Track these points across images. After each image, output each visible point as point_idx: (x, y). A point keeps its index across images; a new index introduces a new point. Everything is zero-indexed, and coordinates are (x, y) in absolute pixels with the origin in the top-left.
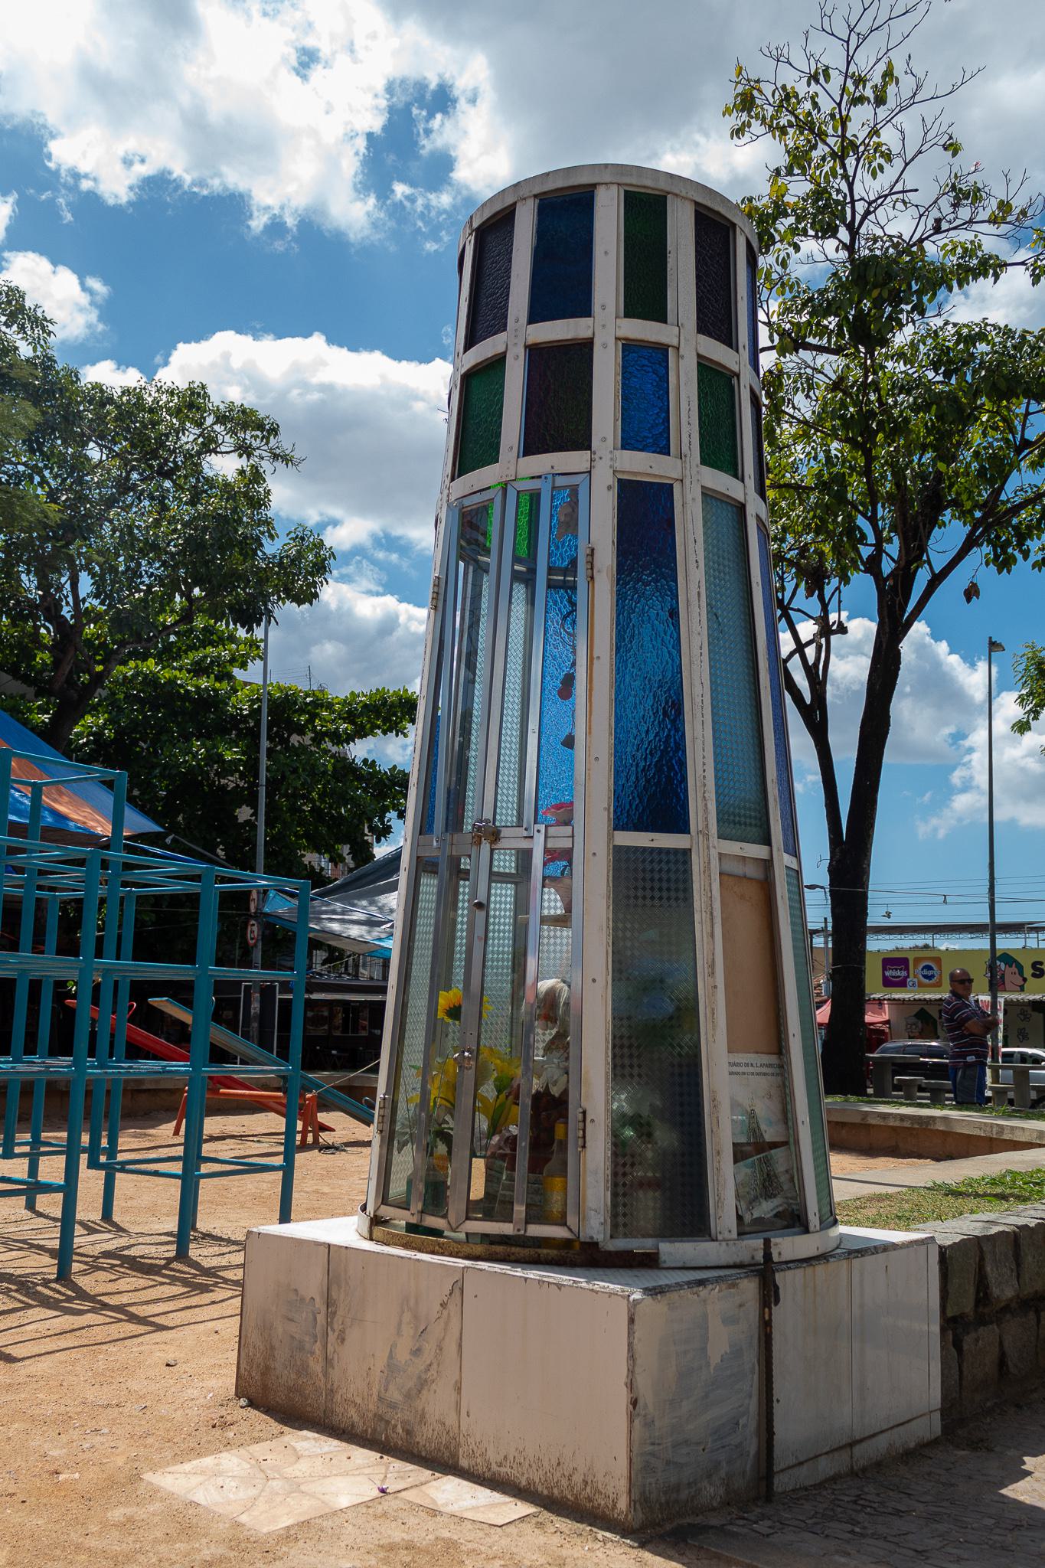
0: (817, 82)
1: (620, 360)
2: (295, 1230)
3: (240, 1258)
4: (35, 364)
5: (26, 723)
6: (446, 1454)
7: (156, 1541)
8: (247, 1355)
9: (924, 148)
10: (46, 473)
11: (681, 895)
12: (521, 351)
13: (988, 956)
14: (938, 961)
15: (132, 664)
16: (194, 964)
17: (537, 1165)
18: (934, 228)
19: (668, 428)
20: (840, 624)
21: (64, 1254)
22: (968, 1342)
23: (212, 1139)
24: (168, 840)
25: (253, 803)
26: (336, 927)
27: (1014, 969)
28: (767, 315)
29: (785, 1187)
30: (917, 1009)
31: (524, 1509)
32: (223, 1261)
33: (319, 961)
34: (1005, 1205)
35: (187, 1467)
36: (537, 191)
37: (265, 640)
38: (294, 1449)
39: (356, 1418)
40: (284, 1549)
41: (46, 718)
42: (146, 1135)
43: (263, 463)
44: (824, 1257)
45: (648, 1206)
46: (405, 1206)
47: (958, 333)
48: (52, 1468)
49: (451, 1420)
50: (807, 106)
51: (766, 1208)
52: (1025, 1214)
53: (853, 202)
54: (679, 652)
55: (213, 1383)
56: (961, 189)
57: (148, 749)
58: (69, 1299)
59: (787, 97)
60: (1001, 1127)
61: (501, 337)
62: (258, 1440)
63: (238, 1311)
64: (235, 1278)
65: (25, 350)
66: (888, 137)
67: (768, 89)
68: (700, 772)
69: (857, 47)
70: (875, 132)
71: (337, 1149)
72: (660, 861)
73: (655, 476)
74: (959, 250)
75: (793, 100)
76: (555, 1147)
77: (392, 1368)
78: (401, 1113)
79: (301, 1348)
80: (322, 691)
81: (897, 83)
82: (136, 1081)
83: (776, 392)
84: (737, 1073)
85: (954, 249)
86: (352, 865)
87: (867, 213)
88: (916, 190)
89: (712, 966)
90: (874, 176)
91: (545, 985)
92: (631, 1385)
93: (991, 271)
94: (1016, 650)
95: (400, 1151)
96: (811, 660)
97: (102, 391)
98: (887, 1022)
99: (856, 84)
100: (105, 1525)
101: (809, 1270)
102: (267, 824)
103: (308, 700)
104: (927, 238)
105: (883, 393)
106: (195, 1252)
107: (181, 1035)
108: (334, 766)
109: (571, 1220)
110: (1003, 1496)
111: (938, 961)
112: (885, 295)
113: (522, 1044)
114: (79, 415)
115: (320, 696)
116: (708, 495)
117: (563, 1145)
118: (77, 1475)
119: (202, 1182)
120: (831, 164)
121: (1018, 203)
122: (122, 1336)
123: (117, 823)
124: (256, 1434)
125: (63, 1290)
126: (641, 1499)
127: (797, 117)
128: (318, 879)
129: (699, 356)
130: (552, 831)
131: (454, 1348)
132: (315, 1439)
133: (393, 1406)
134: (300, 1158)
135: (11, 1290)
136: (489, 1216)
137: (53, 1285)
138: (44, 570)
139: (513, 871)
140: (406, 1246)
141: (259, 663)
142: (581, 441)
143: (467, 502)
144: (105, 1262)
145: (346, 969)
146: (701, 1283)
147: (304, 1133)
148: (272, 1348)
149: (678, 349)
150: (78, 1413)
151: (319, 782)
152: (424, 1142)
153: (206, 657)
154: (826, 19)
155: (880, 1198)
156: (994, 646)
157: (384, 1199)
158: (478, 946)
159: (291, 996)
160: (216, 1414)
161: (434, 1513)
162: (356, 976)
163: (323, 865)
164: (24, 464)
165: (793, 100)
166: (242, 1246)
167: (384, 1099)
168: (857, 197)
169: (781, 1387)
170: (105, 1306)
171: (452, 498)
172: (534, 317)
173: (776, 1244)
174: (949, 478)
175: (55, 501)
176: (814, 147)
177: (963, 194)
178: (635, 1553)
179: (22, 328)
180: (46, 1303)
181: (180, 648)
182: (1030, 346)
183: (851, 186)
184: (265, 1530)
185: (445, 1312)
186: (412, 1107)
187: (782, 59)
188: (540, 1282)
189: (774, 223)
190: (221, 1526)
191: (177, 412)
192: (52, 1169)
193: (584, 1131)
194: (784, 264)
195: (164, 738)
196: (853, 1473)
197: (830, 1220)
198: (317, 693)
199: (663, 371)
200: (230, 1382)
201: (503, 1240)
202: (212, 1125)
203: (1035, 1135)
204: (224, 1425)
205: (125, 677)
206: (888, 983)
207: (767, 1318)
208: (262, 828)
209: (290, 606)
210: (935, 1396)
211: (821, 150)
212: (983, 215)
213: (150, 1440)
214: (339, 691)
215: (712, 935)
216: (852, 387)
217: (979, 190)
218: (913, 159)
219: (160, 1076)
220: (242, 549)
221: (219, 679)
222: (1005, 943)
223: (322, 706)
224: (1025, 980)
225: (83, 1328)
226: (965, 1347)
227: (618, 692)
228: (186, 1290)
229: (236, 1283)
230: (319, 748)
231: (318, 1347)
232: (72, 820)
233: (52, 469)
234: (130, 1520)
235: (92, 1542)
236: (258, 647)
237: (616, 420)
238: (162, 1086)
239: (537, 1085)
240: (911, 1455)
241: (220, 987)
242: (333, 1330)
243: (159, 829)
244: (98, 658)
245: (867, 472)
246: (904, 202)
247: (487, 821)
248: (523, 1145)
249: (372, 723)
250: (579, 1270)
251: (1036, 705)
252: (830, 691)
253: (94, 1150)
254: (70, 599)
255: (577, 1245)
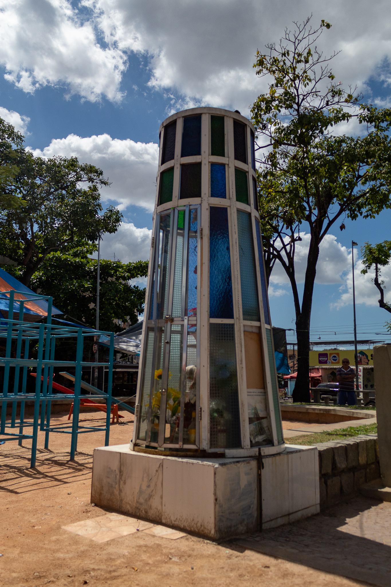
0: (285, 56)
1: (210, 169)
2: (111, 448)
3: (91, 460)
4: (18, 152)
5: (14, 275)
6: (158, 519)
7: (66, 545)
8: (94, 490)
9: (322, 77)
10: (22, 189)
11: (231, 338)
12: (179, 166)
13: (355, 352)
14: (338, 354)
15: (52, 253)
16: (75, 361)
17: (186, 426)
18: (326, 104)
19: (226, 190)
20: (299, 237)
21: (33, 460)
22: (329, 482)
23: (82, 421)
24: (65, 317)
25: (95, 302)
26: (124, 347)
27: (365, 357)
28: (270, 133)
29: (267, 431)
30: (331, 371)
31: (182, 534)
32: (86, 461)
33: (119, 357)
34: (345, 437)
35: (75, 524)
36: (183, 115)
37: (99, 244)
38: (110, 519)
39: (129, 508)
40: (107, 547)
41: (21, 273)
42: (58, 420)
43: (97, 184)
44: (279, 454)
45: (222, 438)
46: (145, 440)
47: (336, 140)
48: (32, 525)
49: (159, 508)
50: (282, 63)
51: (260, 438)
52: (351, 440)
53: (298, 96)
54: (230, 261)
55: (83, 499)
56: (334, 91)
57: (57, 283)
58: (35, 474)
59: (275, 61)
60: (353, 412)
61: (172, 161)
62: (98, 516)
63: (91, 477)
64: (90, 467)
65: (14, 147)
66: (310, 73)
67: (268, 58)
68: (237, 299)
69: (298, 44)
70: (305, 72)
71: (125, 424)
72: (224, 328)
73: (221, 205)
74: (335, 111)
75: (277, 62)
76: (192, 420)
77: (141, 492)
78: (143, 410)
79: (112, 486)
80: (119, 262)
81: (312, 56)
82: (54, 401)
83: (273, 160)
84: (251, 395)
85: (333, 111)
86: (130, 323)
87: (303, 99)
88: (320, 92)
89: (242, 361)
90: (305, 86)
91: (189, 368)
92: (215, 494)
93: (346, 118)
94: (362, 244)
95: (143, 422)
96: (288, 251)
97: (41, 160)
98: (321, 376)
99: (298, 56)
100: (50, 541)
101: (274, 458)
102: (100, 309)
103: (114, 265)
104: (325, 107)
105: (310, 160)
106: (76, 458)
107: (70, 385)
108: (124, 288)
109: (197, 443)
110: (338, 530)
111: (338, 354)
112: (309, 127)
113: (182, 386)
114: (33, 169)
115: (119, 264)
116: (239, 211)
117: (195, 419)
118: (40, 527)
119: (79, 434)
120: (291, 82)
121: (355, 95)
122: (53, 485)
123: (49, 311)
124: (97, 514)
125: (33, 471)
126: (218, 530)
127: (278, 68)
128: (118, 329)
129: (235, 167)
130: (190, 318)
131: (160, 485)
132: (116, 515)
133: (141, 504)
134: (112, 427)
135: (15, 471)
136: (172, 442)
137: (29, 470)
138: (21, 222)
139: (180, 330)
140: (145, 452)
141: (97, 252)
142: (198, 195)
143: (162, 213)
144: (47, 462)
145: (129, 360)
146: (238, 462)
147: (113, 418)
148: (102, 487)
149: (228, 165)
150: (40, 509)
151: (118, 294)
152: (151, 419)
153: (78, 251)
154: (287, 35)
155: (304, 436)
156: (354, 244)
157: (138, 437)
158: (167, 355)
159: (108, 370)
160: (84, 509)
161: (154, 536)
162: (132, 362)
163: (120, 323)
164: (14, 186)
165: (277, 62)
166: (92, 456)
167: (138, 405)
168: (299, 93)
169: (265, 496)
170: (47, 476)
171: (158, 212)
172: (183, 155)
173: (263, 450)
174: (334, 188)
175: (25, 199)
176: (285, 77)
177: (336, 93)
178: (216, 547)
179: (13, 139)
180: (27, 475)
181: (68, 248)
182: (359, 144)
183: (297, 90)
184: (100, 542)
185: (157, 473)
186: (147, 407)
187: (273, 48)
188: (187, 463)
189: (271, 104)
190: (87, 541)
191: (67, 167)
192: (28, 431)
193: (201, 414)
194: (275, 116)
195: (64, 279)
196: (289, 524)
197: (282, 441)
198: (118, 263)
199: (224, 172)
200: (88, 498)
201: (176, 450)
202: (82, 416)
203: (364, 415)
204: (87, 512)
205: (49, 258)
206: (320, 362)
207: (260, 473)
208: (98, 311)
209: (107, 233)
210: (318, 501)
211: (287, 78)
212: (343, 100)
213: (63, 517)
214: (125, 261)
215: (241, 351)
216: (299, 158)
217: (341, 91)
218: (318, 81)
219: (64, 399)
220: (90, 214)
221: (82, 258)
222: (360, 347)
223: (119, 267)
224: (369, 360)
225: (40, 483)
226: (328, 484)
227: (210, 274)
228: (74, 471)
229: (90, 468)
230: (118, 282)
231: (117, 486)
232: (32, 311)
233: (24, 188)
234: (58, 540)
235: (46, 546)
236: (96, 247)
237: (209, 188)
238: (64, 403)
239: (187, 400)
240: (313, 516)
241: (84, 368)
242: (122, 480)
243: (61, 313)
244: (40, 251)
245: (305, 187)
246: (316, 95)
247: (169, 315)
248: (182, 419)
249: (136, 273)
250: (199, 459)
251: (369, 264)
252: (296, 259)
253: (42, 425)
254: (30, 232)
255: (199, 451)
